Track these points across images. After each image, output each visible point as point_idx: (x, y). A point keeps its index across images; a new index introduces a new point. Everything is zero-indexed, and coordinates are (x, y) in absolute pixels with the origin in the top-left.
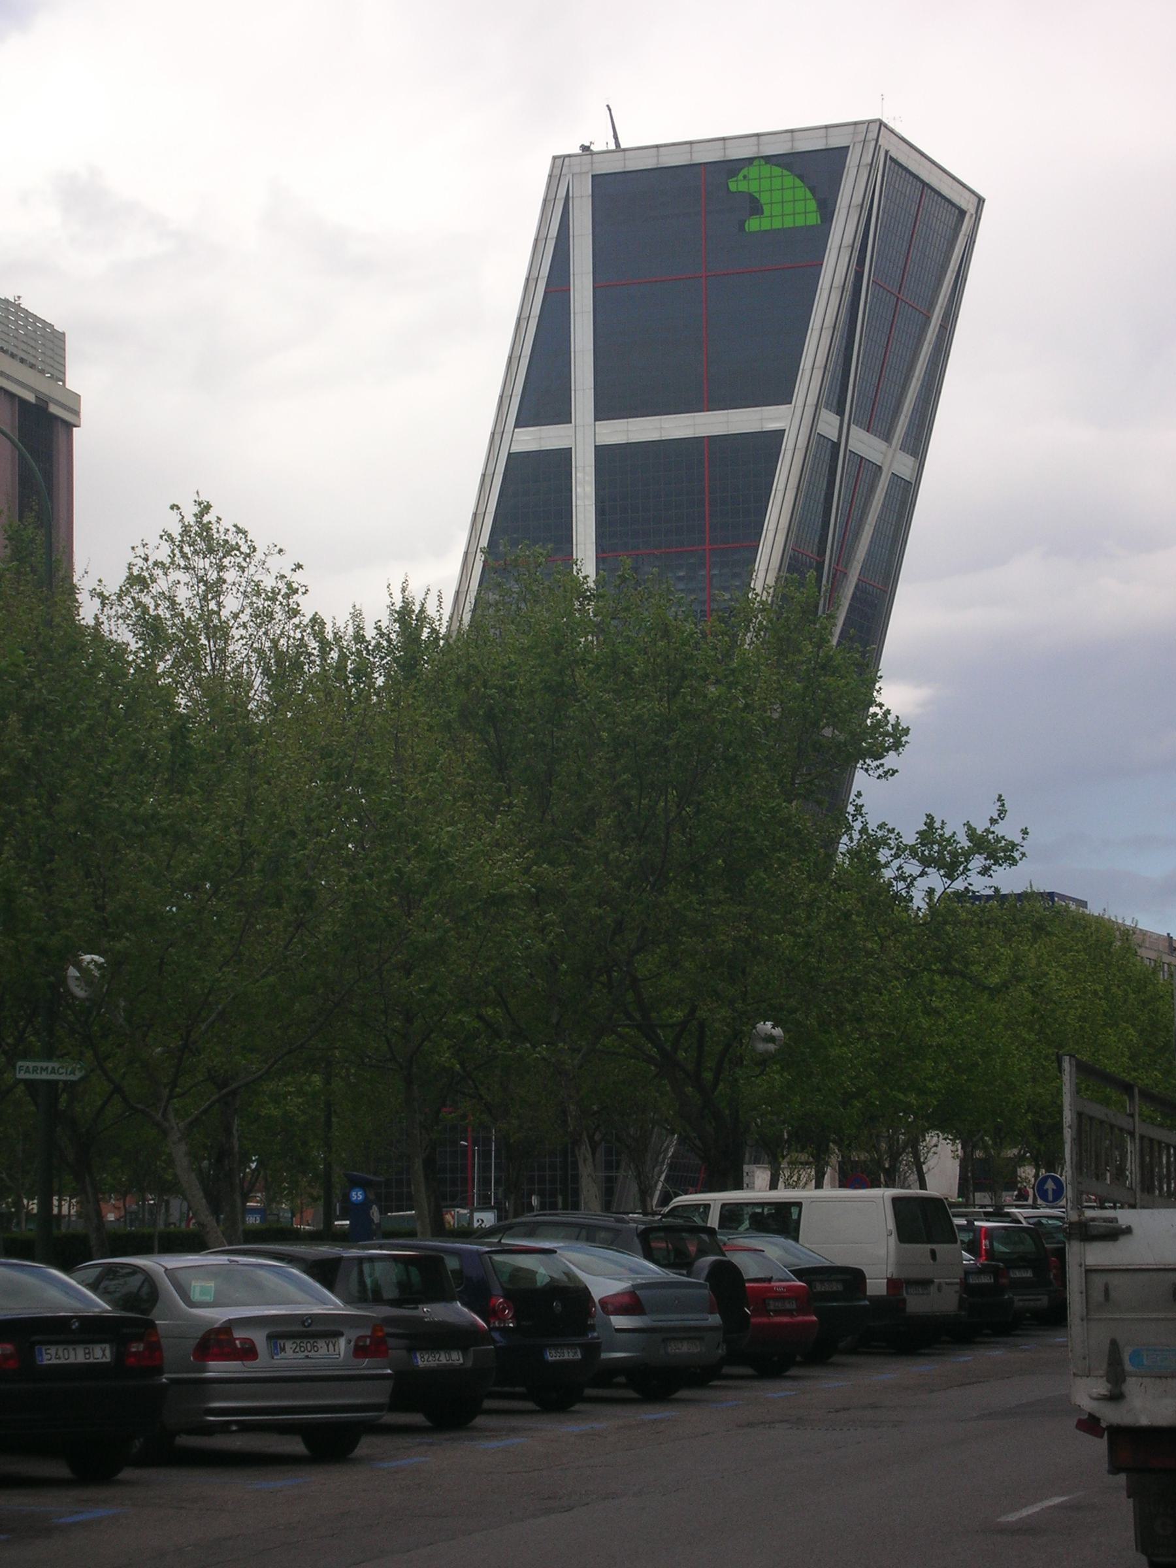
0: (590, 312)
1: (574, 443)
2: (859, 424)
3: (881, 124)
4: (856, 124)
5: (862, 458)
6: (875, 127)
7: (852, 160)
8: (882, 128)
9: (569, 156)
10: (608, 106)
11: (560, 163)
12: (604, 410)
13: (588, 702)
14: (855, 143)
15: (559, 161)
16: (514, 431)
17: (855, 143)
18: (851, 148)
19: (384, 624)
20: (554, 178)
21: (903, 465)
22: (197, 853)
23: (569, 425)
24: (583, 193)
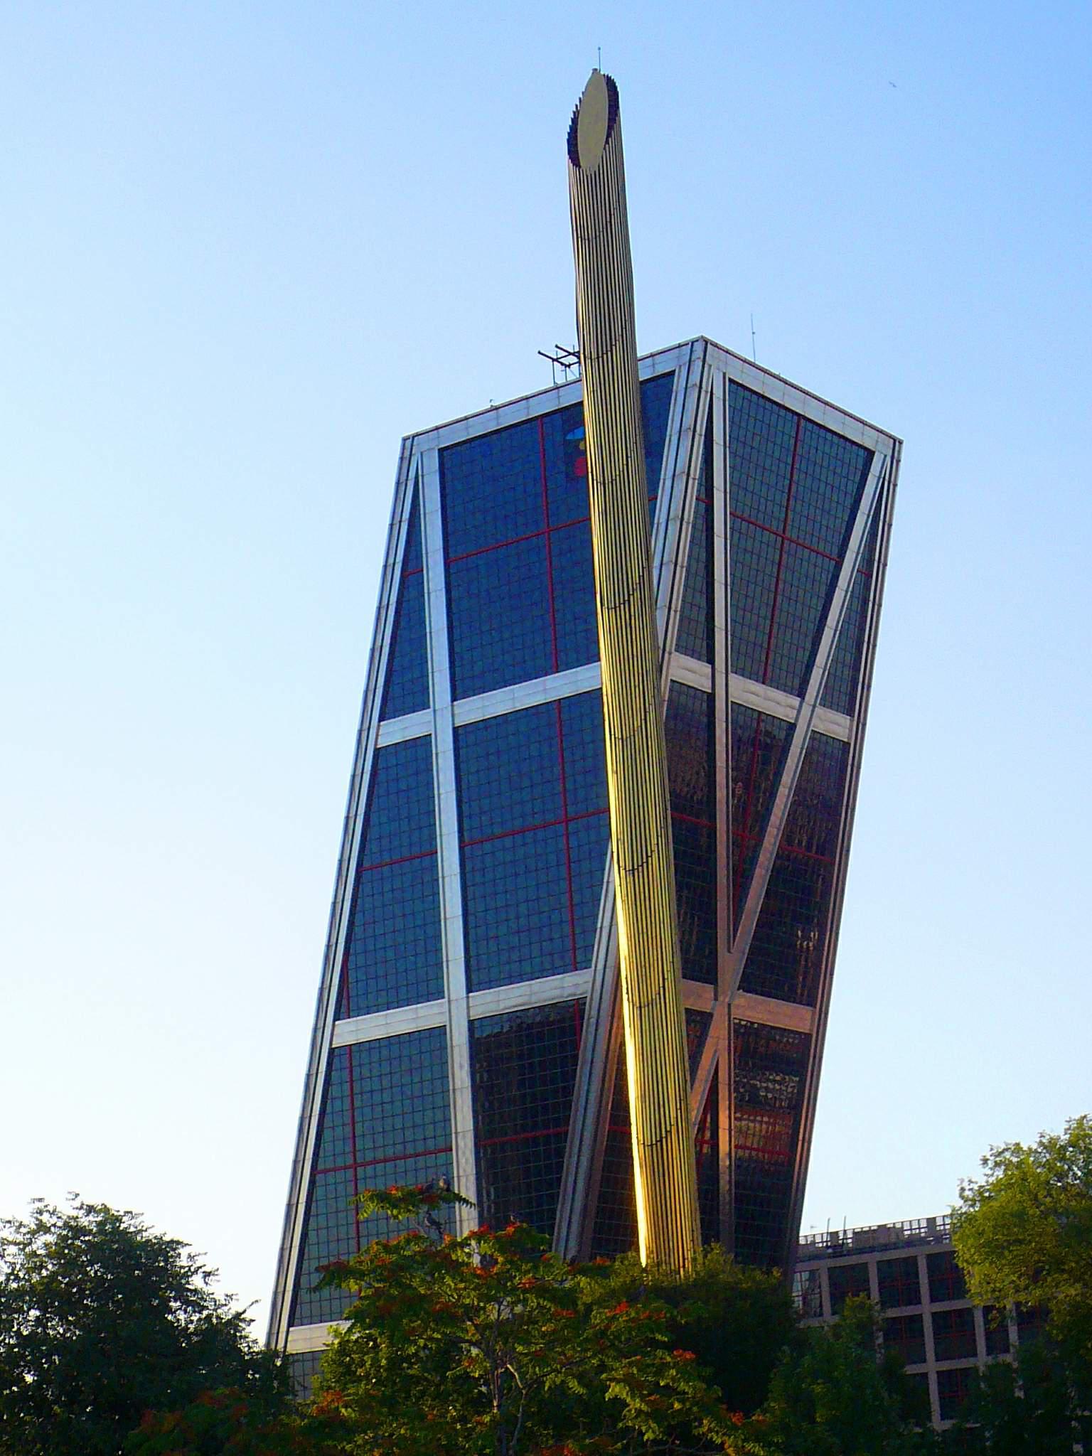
0: (441, 590)
1: (433, 729)
2: (740, 671)
3: (706, 342)
4: (680, 346)
5: (760, 712)
6: (699, 348)
7: (679, 383)
8: (709, 345)
9: (418, 435)
10: (539, 353)
11: (409, 442)
12: (933, 1299)
13: (520, 1199)
14: (680, 366)
15: (408, 443)
16: (468, 997)
17: (680, 366)
18: (677, 372)
19: (230, 1311)
20: (405, 460)
21: (834, 724)
22: (37, 1318)
23: (428, 711)
24: (433, 463)
